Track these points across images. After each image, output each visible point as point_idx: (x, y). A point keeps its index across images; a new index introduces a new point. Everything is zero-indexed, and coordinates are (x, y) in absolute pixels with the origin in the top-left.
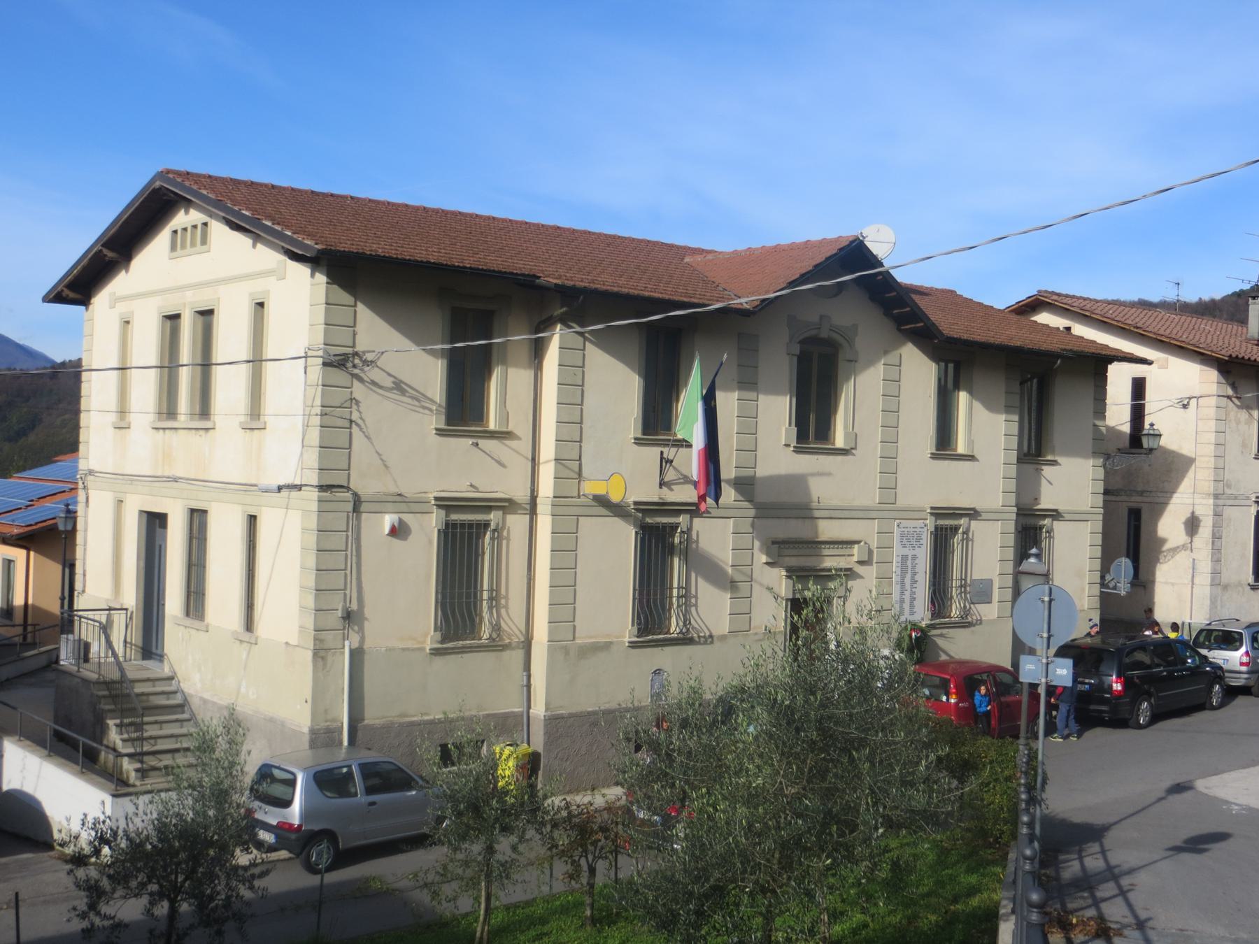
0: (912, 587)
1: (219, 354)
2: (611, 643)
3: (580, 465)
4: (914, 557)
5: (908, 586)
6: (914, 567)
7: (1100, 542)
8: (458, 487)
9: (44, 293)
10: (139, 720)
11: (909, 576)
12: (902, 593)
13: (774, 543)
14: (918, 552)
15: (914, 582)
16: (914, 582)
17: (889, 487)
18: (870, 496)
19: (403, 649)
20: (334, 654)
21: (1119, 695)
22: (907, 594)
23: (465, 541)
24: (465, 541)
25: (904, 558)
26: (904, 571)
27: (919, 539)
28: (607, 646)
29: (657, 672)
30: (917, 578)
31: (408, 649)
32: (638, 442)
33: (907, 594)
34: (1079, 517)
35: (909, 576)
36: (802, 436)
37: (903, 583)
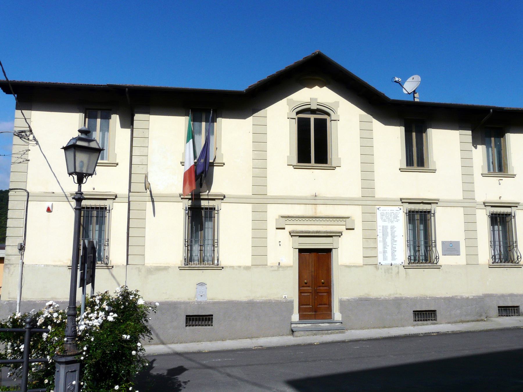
1: (310, 213)
2: (169, 267)
7: (9, 211)
8: (493, 198)
9: (15, 106)
12: (385, 247)
14: (395, 224)
15: (393, 241)
16: (393, 241)
18: (356, 192)
19: (54, 266)
20: (15, 267)
21: (37, 325)
23: (420, 219)
24: (420, 219)
25: (385, 228)
26: (385, 235)
27: (396, 217)
28: (166, 268)
29: (201, 284)
31: (57, 266)
36: (409, 162)
37: (385, 243)
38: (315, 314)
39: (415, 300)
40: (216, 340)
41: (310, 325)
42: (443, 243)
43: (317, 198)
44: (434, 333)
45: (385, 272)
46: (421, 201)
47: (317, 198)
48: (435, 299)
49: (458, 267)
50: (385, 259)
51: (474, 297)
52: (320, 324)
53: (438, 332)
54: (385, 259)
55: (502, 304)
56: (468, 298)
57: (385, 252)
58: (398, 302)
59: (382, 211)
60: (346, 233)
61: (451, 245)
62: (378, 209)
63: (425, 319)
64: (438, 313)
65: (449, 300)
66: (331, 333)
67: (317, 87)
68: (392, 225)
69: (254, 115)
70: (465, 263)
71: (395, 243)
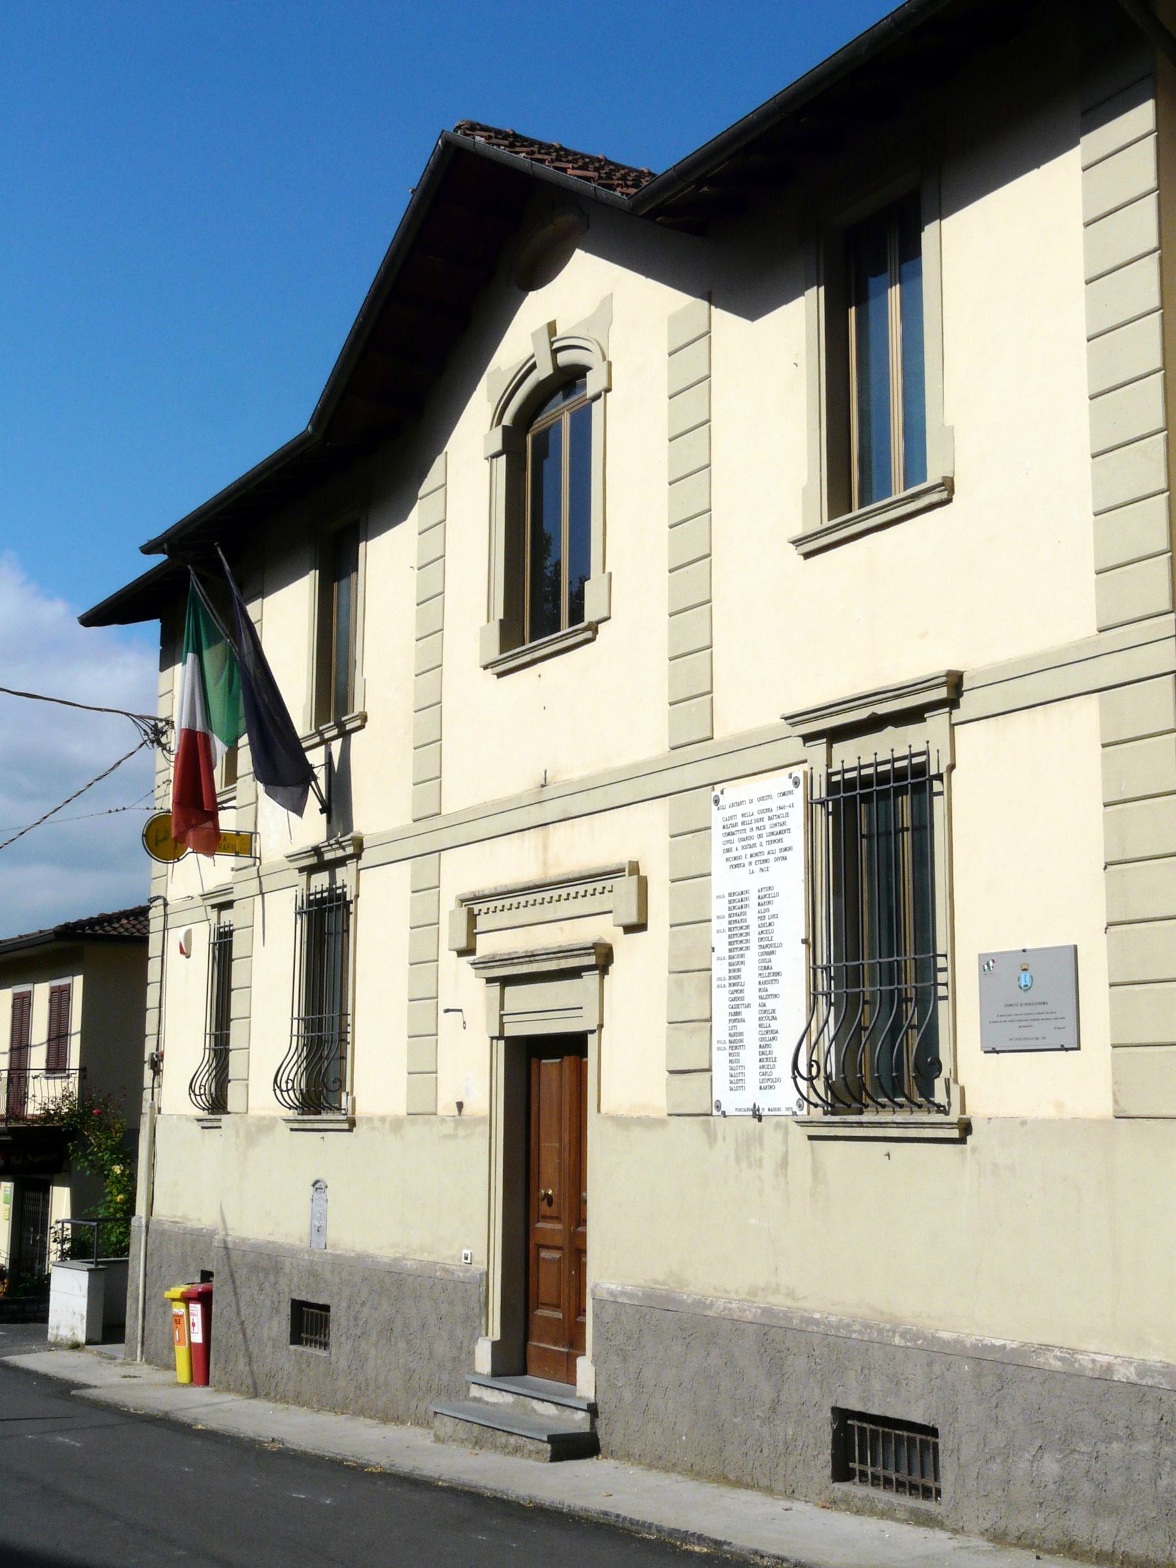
0: (765, 995)
1: (531, 873)
3: (502, 1007)
4: (767, 896)
5: (751, 993)
6: (766, 927)
10: (13, 1125)
11: (752, 957)
12: (736, 1017)
13: (463, 901)
15: (769, 975)
16: (769, 975)
17: (692, 696)
22: (751, 1016)
25: (738, 900)
26: (738, 944)
30: (777, 963)
32: (589, 369)
33: (751, 1016)
34: (1039, 685)
35: (752, 957)
37: (735, 983)
38: (568, 1353)
39: (837, 1345)
40: (339, 1407)
41: (509, 1398)
42: (988, 964)
43: (547, 793)
44: (701, 1539)
45: (738, 1160)
46: (862, 714)
47: (547, 793)
48: (936, 1353)
49: (1063, 1130)
50: (736, 1083)
51: (1144, 1369)
52: (536, 1404)
53: (718, 1543)
54: (736, 1083)
55: (841, 1405)
56: (1104, 1377)
57: (736, 1042)
58: (774, 1339)
59: (729, 812)
60: (625, 948)
61: (1025, 979)
62: (717, 802)
63: (903, 1476)
64: (944, 1442)
65: (1001, 1371)
66: (517, 1450)
67: (923, 234)
68: (764, 880)
69: (421, 493)
70: (1105, 1108)
71: (772, 989)
